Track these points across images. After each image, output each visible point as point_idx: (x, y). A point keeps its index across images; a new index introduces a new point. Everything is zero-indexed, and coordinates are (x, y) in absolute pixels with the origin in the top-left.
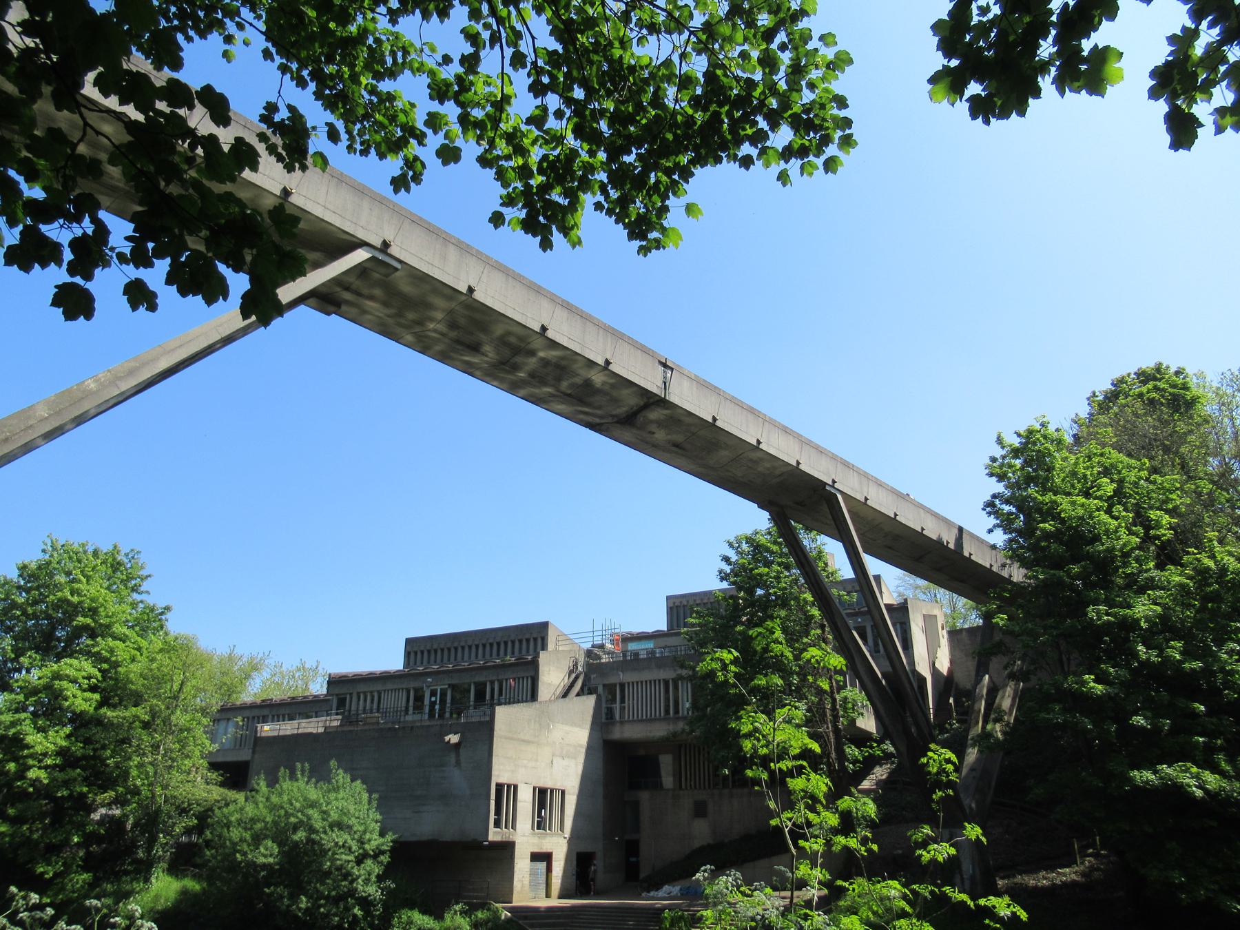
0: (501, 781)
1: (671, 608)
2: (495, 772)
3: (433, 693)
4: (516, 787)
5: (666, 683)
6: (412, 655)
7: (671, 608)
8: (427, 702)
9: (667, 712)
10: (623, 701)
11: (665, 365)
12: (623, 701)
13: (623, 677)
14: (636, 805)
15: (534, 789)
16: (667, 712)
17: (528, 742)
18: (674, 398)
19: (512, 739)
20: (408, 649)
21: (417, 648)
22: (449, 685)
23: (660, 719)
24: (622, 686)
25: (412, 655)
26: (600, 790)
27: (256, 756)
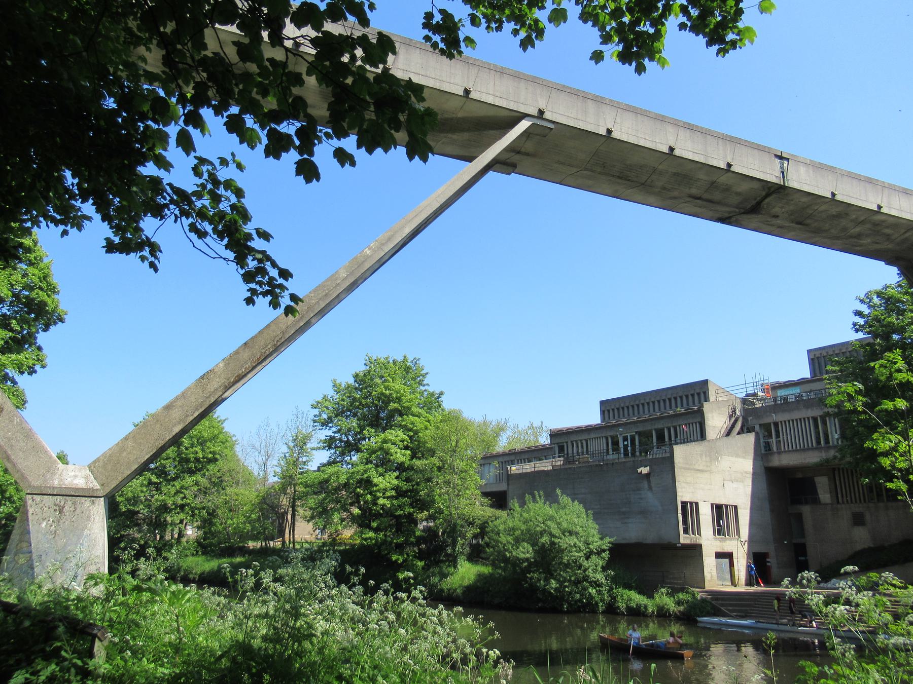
0: (684, 500)
1: (813, 359)
2: (679, 494)
3: (625, 439)
4: (697, 504)
5: (815, 419)
6: (606, 413)
7: (813, 359)
8: (621, 445)
9: (819, 442)
10: (778, 436)
11: (781, 157)
12: (778, 436)
13: (775, 418)
14: (799, 517)
15: (712, 505)
16: (819, 442)
17: (702, 471)
19: (689, 469)
20: (603, 409)
22: (636, 432)
23: (813, 449)
24: (776, 424)
25: (606, 413)
26: (767, 506)
27: (510, 487)
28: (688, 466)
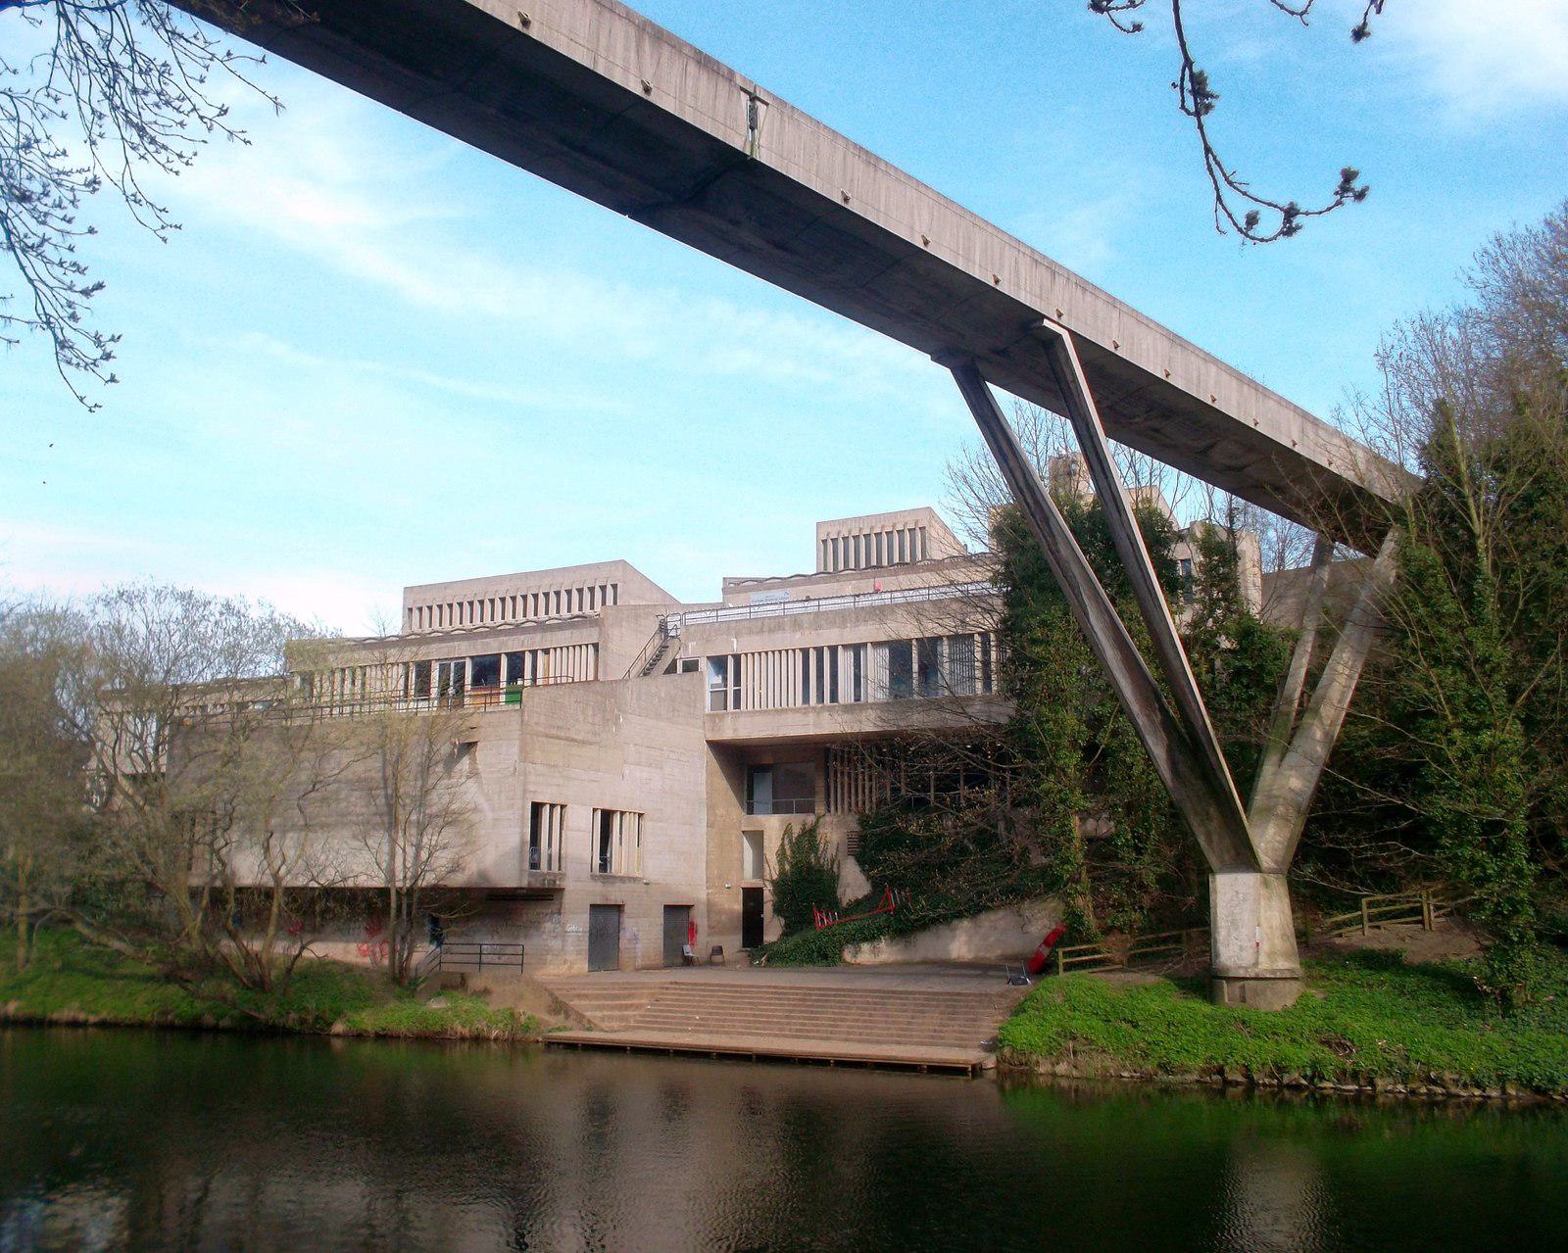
0: (538, 800)
5: (805, 652)
6: (416, 613)
9: (806, 699)
11: (753, 98)
15: (594, 810)
17: (584, 742)
18: (764, 157)
21: (418, 602)
23: (796, 711)
24: (737, 658)
25: (416, 613)
28: (554, 732)
